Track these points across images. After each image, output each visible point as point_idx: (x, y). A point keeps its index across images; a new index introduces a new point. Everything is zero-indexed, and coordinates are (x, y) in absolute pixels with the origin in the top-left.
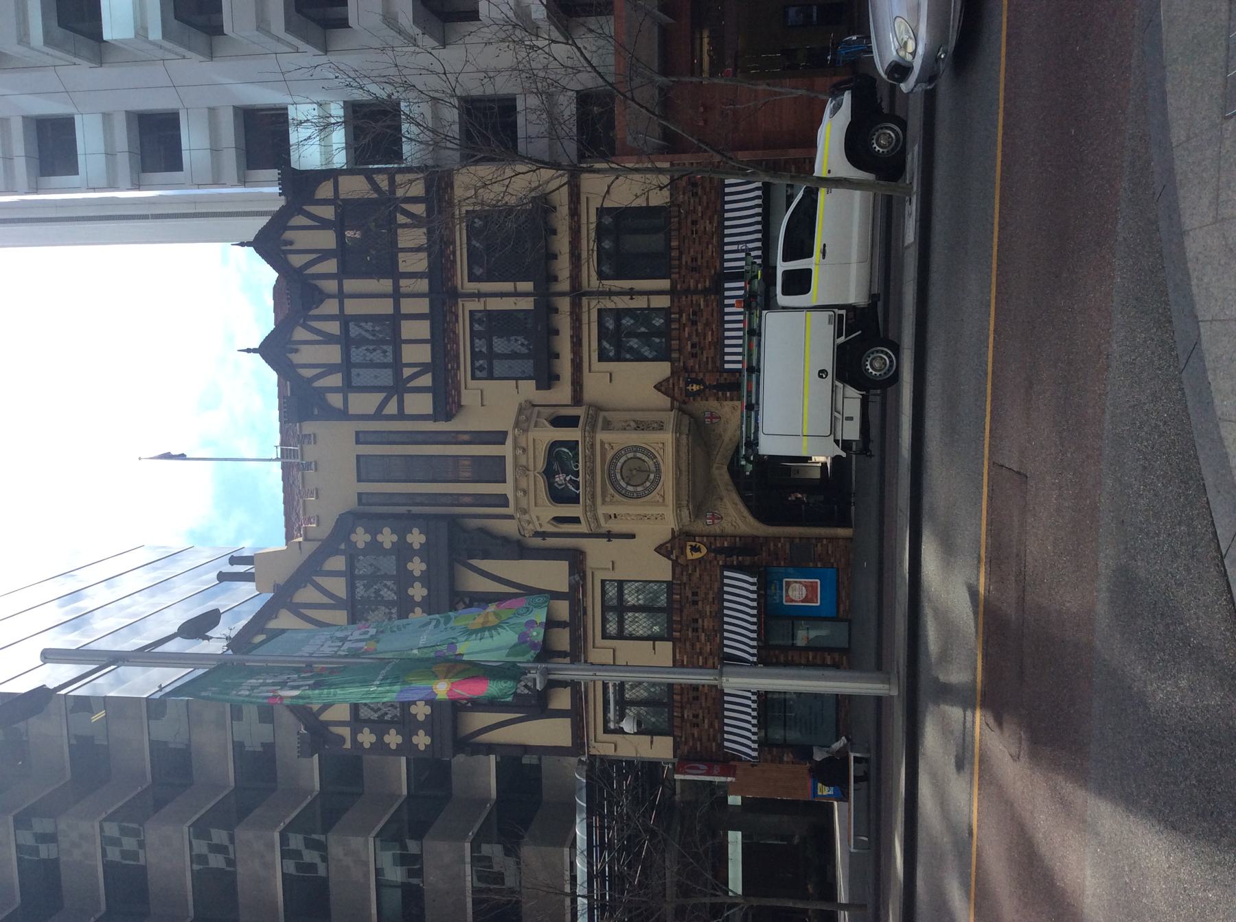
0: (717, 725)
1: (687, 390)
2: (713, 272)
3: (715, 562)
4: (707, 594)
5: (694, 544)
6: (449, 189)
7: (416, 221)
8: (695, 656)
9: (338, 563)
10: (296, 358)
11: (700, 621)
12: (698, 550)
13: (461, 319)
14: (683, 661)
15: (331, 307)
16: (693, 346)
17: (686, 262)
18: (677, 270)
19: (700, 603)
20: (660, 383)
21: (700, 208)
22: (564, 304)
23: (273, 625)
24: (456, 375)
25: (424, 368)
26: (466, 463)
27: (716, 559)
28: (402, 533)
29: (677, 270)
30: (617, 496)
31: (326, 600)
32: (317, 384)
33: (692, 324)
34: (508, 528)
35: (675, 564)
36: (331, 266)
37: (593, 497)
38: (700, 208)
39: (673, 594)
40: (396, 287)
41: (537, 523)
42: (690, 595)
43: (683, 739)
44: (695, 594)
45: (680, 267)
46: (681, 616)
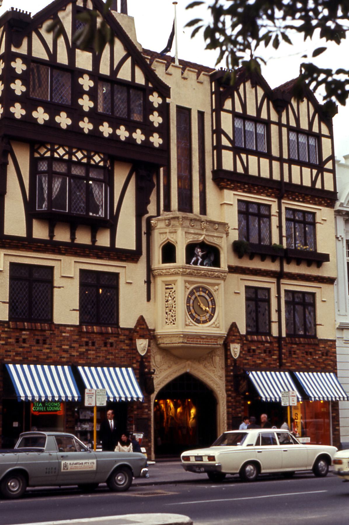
0: (17, 358)
9: (140, 79)
10: (248, 84)
11: (94, 348)
14: (65, 332)
15: (274, 117)
16: (254, 351)
19: (106, 348)
22: (274, 267)
24: (241, 189)
32: (236, 94)
34: (152, 209)
42: (110, 341)
43: (6, 329)
45: (292, 343)
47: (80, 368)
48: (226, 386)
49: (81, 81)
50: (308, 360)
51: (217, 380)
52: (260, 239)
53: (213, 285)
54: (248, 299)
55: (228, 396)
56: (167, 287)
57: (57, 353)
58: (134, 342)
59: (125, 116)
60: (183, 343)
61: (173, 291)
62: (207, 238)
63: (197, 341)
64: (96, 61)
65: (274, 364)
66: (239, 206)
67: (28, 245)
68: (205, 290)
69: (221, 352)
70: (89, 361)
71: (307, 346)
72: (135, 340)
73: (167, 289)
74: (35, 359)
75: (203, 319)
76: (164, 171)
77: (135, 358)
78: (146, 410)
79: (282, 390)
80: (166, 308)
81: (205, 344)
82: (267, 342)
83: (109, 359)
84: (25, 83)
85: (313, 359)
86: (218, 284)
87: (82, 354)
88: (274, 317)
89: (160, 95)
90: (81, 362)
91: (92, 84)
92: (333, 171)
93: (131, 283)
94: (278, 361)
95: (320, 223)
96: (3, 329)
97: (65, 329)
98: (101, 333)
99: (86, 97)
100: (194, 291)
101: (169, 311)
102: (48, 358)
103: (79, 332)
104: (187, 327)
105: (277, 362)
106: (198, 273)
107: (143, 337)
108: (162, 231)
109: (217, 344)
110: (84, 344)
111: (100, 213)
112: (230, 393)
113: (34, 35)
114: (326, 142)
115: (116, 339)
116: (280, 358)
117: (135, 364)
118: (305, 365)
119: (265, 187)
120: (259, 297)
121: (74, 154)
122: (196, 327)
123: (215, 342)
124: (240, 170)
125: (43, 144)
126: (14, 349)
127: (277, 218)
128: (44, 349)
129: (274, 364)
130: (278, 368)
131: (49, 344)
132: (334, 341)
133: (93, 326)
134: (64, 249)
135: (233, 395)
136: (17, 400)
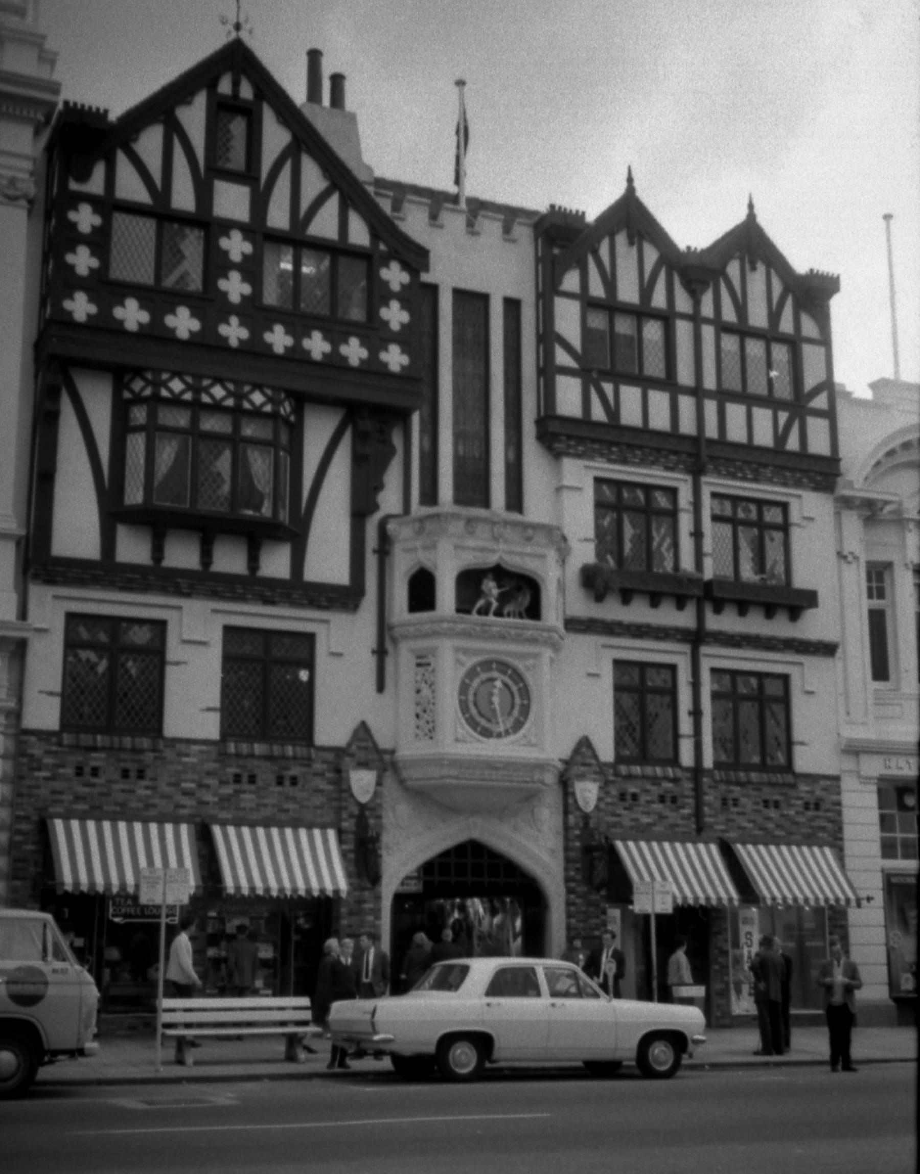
4: (293, 799)
7: (781, 438)
10: (621, 239)
11: (252, 787)
13: (612, 466)
15: (683, 303)
16: (635, 797)
19: (279, 789)
22: (685, 619)
23: (269, 118)
24: (602, 455)
25: (613, 412)
28: (405, 338)
31: (305, 204)
35: (339, 752)
43: (54, 748)
44: (294, 781)
47: (217, 830)
48: (566, 870)
49: (224, 243)
50: (768, 818)
51: (546, 857)
52: (676, 567)
53: (523, 656)
54: (619, 688)
55: (570, 891)
56: (419, 661)
57: (168, 797)
58: (344, 775)
59: (325, 311)
60: (457, 778)
62: (507, 558)
64: (259, 204)
66: (598, 491)
68: (504, 667)
69: (552, 798)
70: (241, 814)
71: (766, 789)
72: (347, 772)
73: (419, 665)
74: (118, 809)
76: (422, 421)
79: (143, 862)
82: (666, 778)
83: (287, 811)
84: (406, 304)
85: (782, 816)
86: (536, 656)
88: (686, 725)
90: (224, 815)
91: (248, 248)
92: (830, 414)
93: (339, 655)
94: (693, 819)
98: (270, 758)
99: (235, 276)
100: (479, 669)
102: (148, 806)
103: (220, 754)
104: (460, 745)
107: (364, 765)
108: (409, 545)
109: (533, 782)
111: (264, 510)
112: (573, 885)
113: (122, 160)
114: (811, 355)
115: (304, 769)
116: (698, 814)
117: (346, 820)
118: (762, 828)
119: (658, 450)
120: (649, 684)
121: (206, 390)
122: (477, 745)
124: (598, 413)
125: (138, 372)
130: (694, 833)
132: (837, 779)
133: (252, 743)
136: (54, 891)
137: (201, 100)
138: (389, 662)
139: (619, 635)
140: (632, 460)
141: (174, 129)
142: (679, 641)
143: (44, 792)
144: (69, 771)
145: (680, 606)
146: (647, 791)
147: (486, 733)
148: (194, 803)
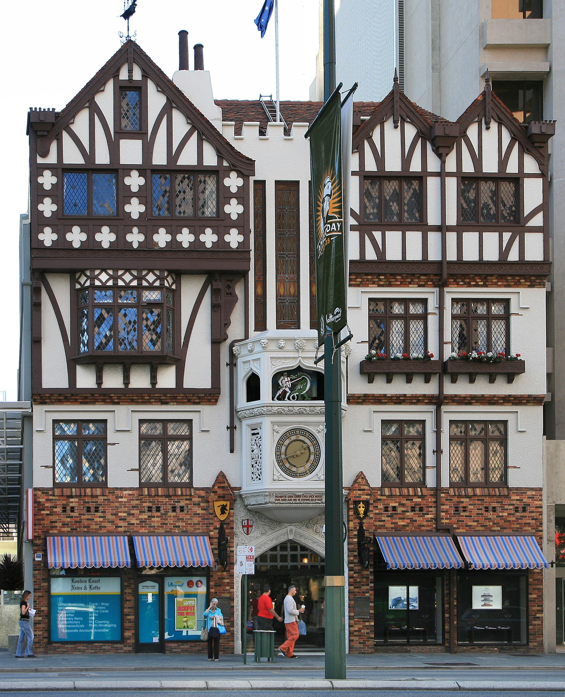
1: (359, 502)
2: (455, 526)
3: (211, 528)
5: (228, 508)
6: (529, 284)
7: (504, 253)
8: (127, 510)
10: (389, 125)
11: (159, 514)
12: (223, 512)
14: (122, 497)
15: (433, 164)
16: (394, 508)
17: (463, 502)
18: (457, 493)
19: (174, 514)
20: (364, 478)
21: (506, 514)
22: (431, 389)
23: (151, 87)
24: (374, 283)
25: (381, 252)
26: (292, 291)
27: (215, 529)
29: (457, 493)
30: (279, 436)
33: (412, 507)
36: (468, 167)
37: (280, 414)
38: (506, 514)
39: (181, 488)
40: (450, 229)
41: (250, 358)
43: (51, 497)
45: (460, 496)
46: (162, 496)
56: (253, 432)
57: (112, 522)
61: (259, 438)
63: (291, 500)
64: (148, 151)
65: (428, 526)
67: (72, 398)
71: (487, 499)
73: (253, 434)
75: (302, 470)
77: (212, 524)
78: (228, 588)
80: (252, 459)
81: (304, 503)
87: (142, 521)
89: (240, 174)
91: (142, 181)
95: (517, 314)
96: (47, 497)
97: (122, 493)
101: (255, 462)
104: (275, 483)
105: (433, 524)
106: (289, 411)
110: (146, 510)
112: (352, 565)
117: (212, 531)
123: (319, 500)
125: (83, 272)
126: (61, 519)
127: (437, 317)
128: (97, 517)
129: (428, 526)
131: (102, 512)
134: (116, 398)
135: (357, 568)
137: (110, 87)
138: (237, 433)
139: (385, 403)
140: (395, 283)
141: (95, 110)
142: (427, 404)
143: (46, 522)
144: (59, 510)
145: (427, 381)
146: (403, 505)
147: (294, 475)
148: (126, 524)
